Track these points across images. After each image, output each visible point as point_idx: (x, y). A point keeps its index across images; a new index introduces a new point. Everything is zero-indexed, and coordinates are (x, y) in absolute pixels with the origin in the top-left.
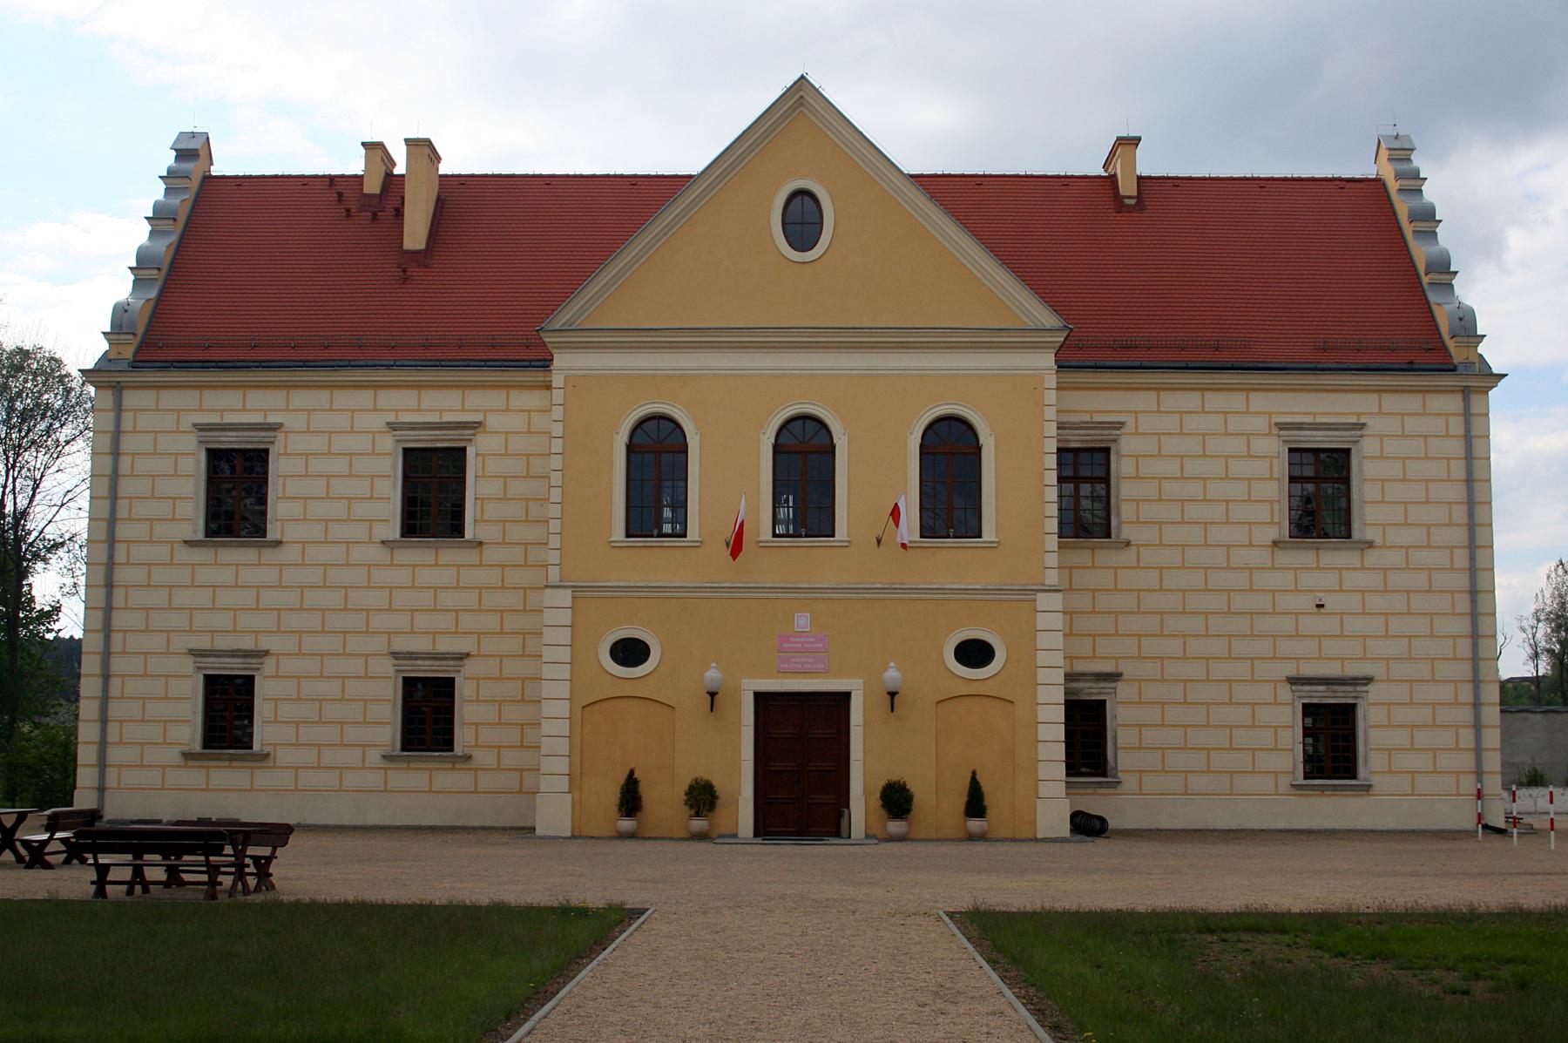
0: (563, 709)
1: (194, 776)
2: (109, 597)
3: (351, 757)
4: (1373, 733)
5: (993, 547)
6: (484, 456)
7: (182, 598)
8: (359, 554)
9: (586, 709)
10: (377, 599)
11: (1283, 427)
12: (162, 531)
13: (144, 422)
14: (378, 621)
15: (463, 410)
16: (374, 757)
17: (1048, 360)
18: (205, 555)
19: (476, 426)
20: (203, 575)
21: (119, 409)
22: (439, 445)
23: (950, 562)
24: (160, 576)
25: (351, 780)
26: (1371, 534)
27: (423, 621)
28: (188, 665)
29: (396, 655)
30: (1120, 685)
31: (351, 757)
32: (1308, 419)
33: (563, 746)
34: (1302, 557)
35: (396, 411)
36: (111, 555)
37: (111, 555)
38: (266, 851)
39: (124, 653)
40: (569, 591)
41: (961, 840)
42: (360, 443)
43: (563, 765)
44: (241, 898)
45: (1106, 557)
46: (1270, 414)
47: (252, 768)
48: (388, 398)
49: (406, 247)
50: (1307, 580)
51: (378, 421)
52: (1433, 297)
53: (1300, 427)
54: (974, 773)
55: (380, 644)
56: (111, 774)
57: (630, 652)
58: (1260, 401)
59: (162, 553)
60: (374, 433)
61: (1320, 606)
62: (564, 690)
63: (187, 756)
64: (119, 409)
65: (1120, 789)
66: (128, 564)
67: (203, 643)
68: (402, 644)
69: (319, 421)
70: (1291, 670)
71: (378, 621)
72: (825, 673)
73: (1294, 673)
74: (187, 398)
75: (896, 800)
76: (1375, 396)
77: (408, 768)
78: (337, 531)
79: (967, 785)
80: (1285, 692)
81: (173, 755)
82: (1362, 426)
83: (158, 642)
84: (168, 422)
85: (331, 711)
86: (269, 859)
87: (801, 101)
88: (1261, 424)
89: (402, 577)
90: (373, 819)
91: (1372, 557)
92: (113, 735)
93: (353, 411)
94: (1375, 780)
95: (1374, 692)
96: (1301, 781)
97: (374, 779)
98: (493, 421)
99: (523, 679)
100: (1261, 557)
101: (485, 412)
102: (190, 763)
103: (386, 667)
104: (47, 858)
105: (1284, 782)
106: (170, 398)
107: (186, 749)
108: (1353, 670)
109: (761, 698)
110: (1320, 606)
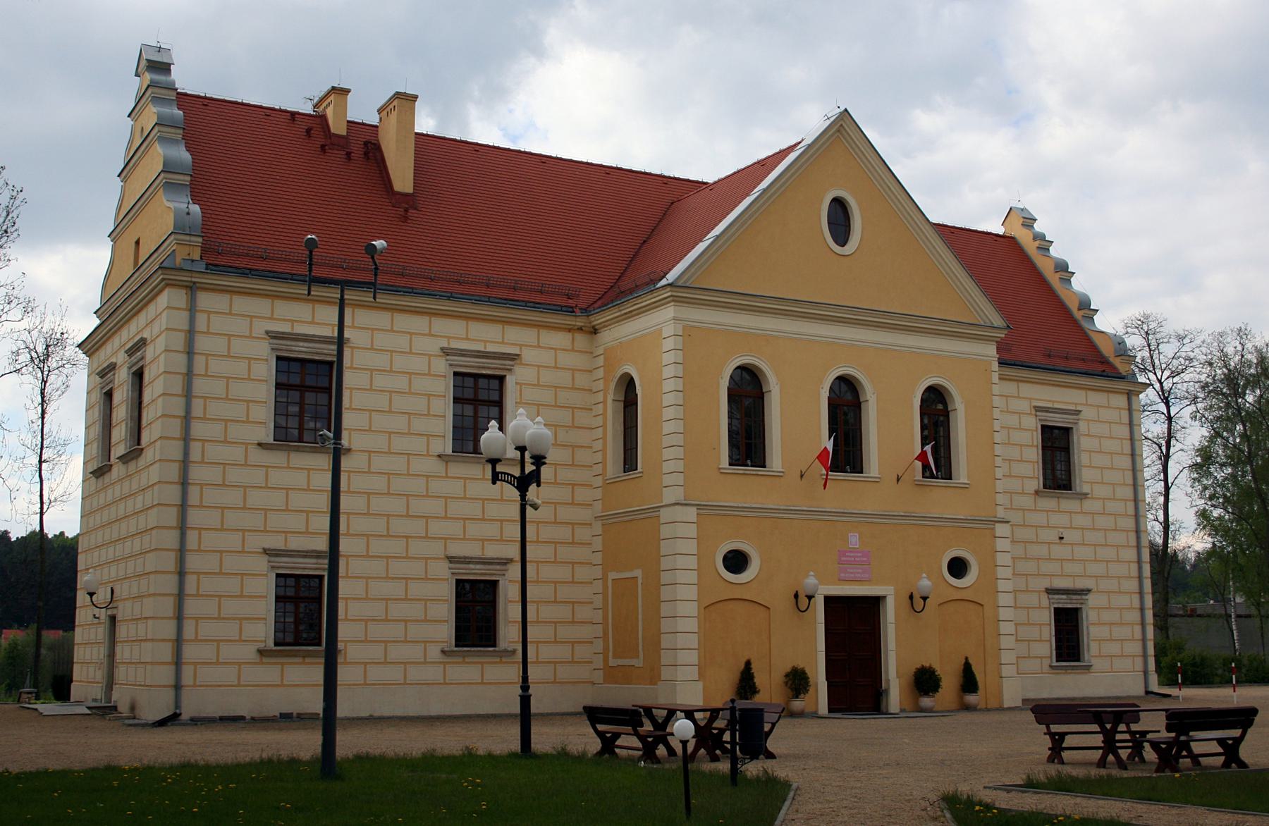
0: (692, 609)
1: (269, 673)
2: (184, 495)
3: (415, 652)
4: (1092, 629)
5: (965, 487)
6: (521, 384)
7: (256, 498)
8: (420, 465)
9: (710, 607)
10: (434, 507)
11: (1038, 409)
12: (236, 432)
13: (218, 323)
14: (436, 528)
15: (503, 343)
16: (434, 652)
17: (991, 350)
18: (278, 458)
19: (514, 357)
20: (277, 478)
21: (192, 309)
22: (484, 372)
23: (939, 500)
24: (234, 475)
25: (415, 674)
26: (1086, 489)
27: (474, 529)
28: (262, 564)
29: (451, 559)
30: (1090, 597)
31: (415, 652)
32: (1050, 405)
33: (693, 641)
34: (1048, 503)
35: (449, 338)
36: (186, 453)
37: (186, 453)
38: (1236, 733)
39: (199, 550)
40: (694, 509)
41: (958, 710)
42: (418, 364)
43: (693, 657)
44: (1116, 772)
45: (1068, 504)
46: (1031, 399)
47: (282, 664)
48: (440, 325)
49: (410, 190)
50: (1055, 519)
51: (434, 345)
52: (1085, 325)
53: (1047, 410)
54: (748, 663)
55: (437, 549)
56: (187, 672)
57: (736, 561)
58: (1027, 390)
59: (236, 454)
60: (430, 355)
61: (1061, 538)
62: (692, 593)
63: (261, 652)
64: (192, 309)
65: (1092, 670)
66: (202, 462)
67: (276, 542)
68: (457, 550)
69: (382, 340)
70: (1046, 583)
71: (436, 528)
72: (868, 581)
73: (1048, 586)
74: (259, 306)
75: (925, 681)
76: (1083, 392)
77: (304, 663)
78: (399, 444)
79: (742, 666)
80: (1045, 600)
81: (249, 652)
82: (1078, 412)
83: (233, 541)
84: (241, 326)
85: (397, 610)
86: (1238, 741)
87: (843, 129)
88: (1024, 406)
89: (455, 488)
90: (435, 710)
91: (1088, 505)
92: (189, 632)
93: (411, 334)
94: (1094, 661)
95: (1092, 600)
96: (1055, 664)
97: (433, 673)
98: (528, 355)
99: (555, 583)
100: (1028, 501)
101: (521, 346)
102: (265, 660)
103: (443, 570)
104: (617, 750)
105: (1046, 662)
106: (243, 304)
107: (262, 646)
108: (1080, 584)
109: (829, 600)
110: (1061, 538)
